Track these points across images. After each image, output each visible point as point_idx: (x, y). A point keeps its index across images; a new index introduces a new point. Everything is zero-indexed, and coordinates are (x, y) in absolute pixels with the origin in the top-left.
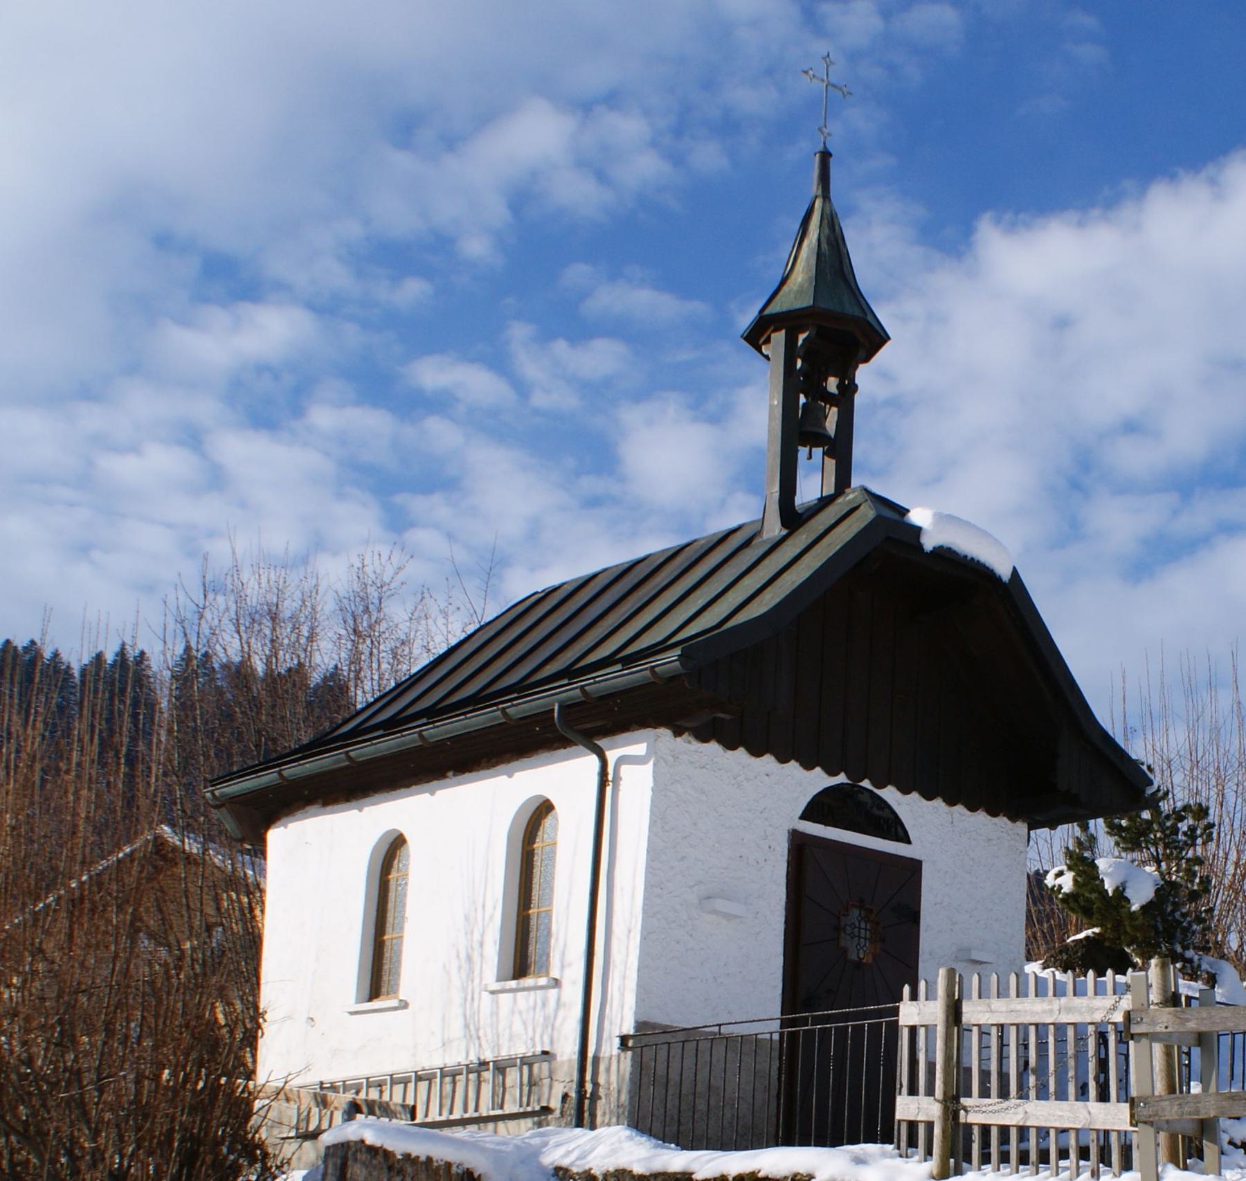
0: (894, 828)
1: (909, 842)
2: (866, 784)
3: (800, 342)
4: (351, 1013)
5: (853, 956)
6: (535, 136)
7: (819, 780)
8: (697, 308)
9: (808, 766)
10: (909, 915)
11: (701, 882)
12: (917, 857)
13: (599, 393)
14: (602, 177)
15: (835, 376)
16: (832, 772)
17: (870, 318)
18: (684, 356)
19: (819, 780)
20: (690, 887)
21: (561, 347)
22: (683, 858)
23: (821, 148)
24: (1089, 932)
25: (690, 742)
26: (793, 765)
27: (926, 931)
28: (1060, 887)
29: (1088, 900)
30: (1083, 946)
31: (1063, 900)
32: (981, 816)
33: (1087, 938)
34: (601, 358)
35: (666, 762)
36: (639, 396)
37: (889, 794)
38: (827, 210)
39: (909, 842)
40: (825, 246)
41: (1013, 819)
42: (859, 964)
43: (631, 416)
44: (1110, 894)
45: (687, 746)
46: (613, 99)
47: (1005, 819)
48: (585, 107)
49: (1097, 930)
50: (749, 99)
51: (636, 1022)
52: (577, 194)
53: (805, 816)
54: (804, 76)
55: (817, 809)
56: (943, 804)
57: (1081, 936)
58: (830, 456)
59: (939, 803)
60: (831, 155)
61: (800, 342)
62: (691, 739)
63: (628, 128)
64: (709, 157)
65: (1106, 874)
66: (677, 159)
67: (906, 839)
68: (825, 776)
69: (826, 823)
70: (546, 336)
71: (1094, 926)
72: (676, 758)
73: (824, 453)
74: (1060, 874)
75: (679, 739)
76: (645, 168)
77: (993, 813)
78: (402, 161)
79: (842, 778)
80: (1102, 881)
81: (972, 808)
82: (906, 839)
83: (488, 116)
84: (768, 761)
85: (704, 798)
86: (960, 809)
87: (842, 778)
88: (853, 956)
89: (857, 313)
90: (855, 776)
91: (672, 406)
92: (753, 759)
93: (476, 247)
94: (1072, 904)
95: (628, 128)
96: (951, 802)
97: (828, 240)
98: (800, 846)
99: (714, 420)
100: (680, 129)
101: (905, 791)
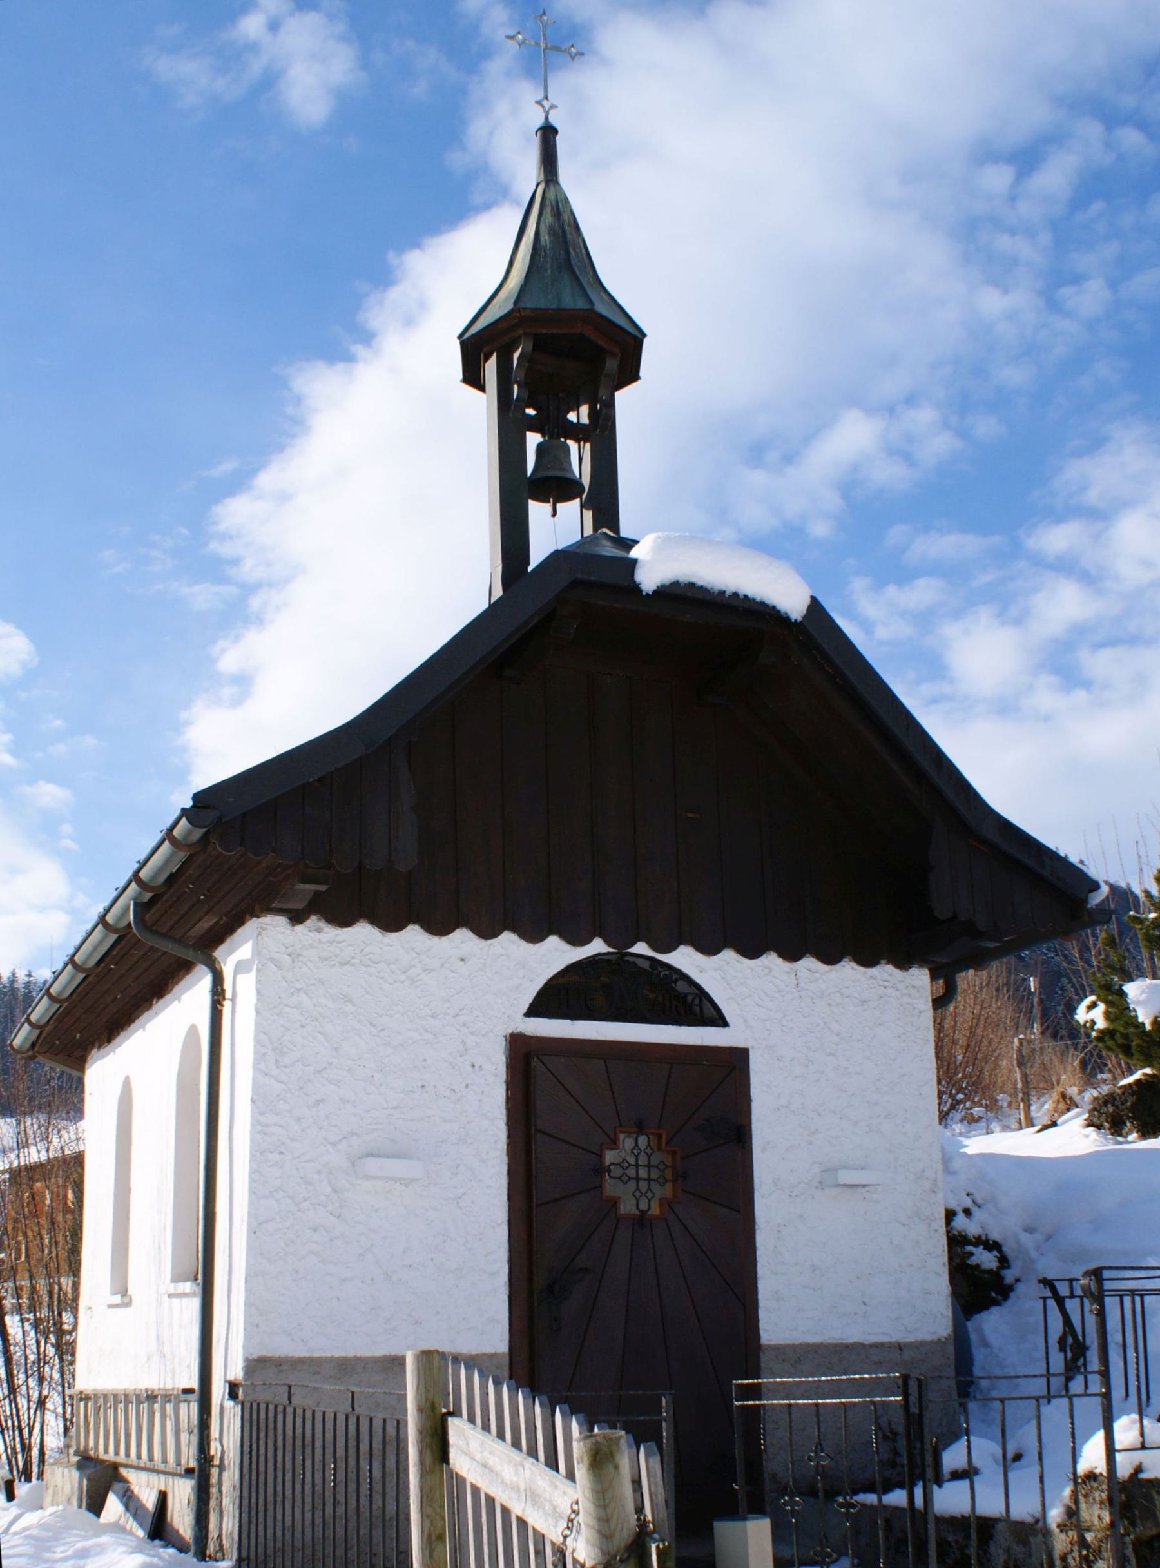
0: (698, 1008)
1: (724, 1023)
2: (641, 948)
3: (515, 362)
4: (110, 1306)
5: (627, 1207)
6: (853, 437)
7: (555, 955)
8: (996, 540)
9: (534, 935)
10: (736, 1134)
11: (352, 1134)
12: (741, 1044)
13: (925, 619)
14: (908, 459)
15: (585, 403)
16: (576, 939)
17: (601, 308)
18: (988, 577)
19: (555, 955)
20: (333, 1144)
21: (891, 590)
22: (318, 1103)
23: (540, 122)
24: (1137, 1075)
25: (319, 930)
26: (508, 939)
27: (764, 1150)
28: (1093, 1023)
29: (1125, 1036)
30: (1134, 1093)
31: (1098, 1039)
32: (848, 969)
33: (1138, 1082)
34: (923, 593)
35: (279, 966)
36: (957, 614)
37: (684, 959)
38: (551, 195)
39: (724, 1023)
40: (545, 238)
41: (903, 964)
42: (641, 1220)
43: (951, 630)
44: (1148, 1027)
45: (316, 935)
46: (911, 400)
47: (890, 968)
48: (890, 410)
49: (1148, 1071)
50: (1014, 376)
51: (246, 1360)
52: (888, 474)
53: (534, 1010)
54: (510, 42)
55: (553, 999)
56: (780, 961)
57: (1130, 1080)
58: (588, 509)
59: (771, 960)
60: (556, 131)
61: (515, 362)
62: (322, 924)
63: (924, 417)
64: (986, 427)
65: (1138, 1003)
66: (963, 434)
67: (719, 1020)
68: (567, 947)
69: (574, 1017)
70: (880, 583)
71: (1143, 1067)
72: (295, 956)
73: (582, 507)
74: (1093, 1006)
75: (299, 928)
76: (939, 445)
77: (867, 961)
78: (759, 478)
79: (597, 946)
80: (1135, 1010)
81: (830, 959)
82: (719, 1020)
83: (818, 428)
84: (462, 937)
85: (349, 1008)
86: (809, 964)
87: (597, 946)
88: (627, 1207)
89: (581, 304)
90: (621, 939)
91: (984, 614)
92: (436, 939)
93: (820, 530)
94: (1110, 1043)
95: (924, 417)
96: (791, 954)
97: (552, 231)
98: (523, 1054)
99: (1018, 622)
100: (961, 407)
101: (709, 948)
